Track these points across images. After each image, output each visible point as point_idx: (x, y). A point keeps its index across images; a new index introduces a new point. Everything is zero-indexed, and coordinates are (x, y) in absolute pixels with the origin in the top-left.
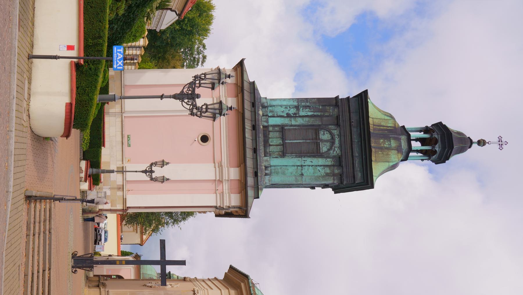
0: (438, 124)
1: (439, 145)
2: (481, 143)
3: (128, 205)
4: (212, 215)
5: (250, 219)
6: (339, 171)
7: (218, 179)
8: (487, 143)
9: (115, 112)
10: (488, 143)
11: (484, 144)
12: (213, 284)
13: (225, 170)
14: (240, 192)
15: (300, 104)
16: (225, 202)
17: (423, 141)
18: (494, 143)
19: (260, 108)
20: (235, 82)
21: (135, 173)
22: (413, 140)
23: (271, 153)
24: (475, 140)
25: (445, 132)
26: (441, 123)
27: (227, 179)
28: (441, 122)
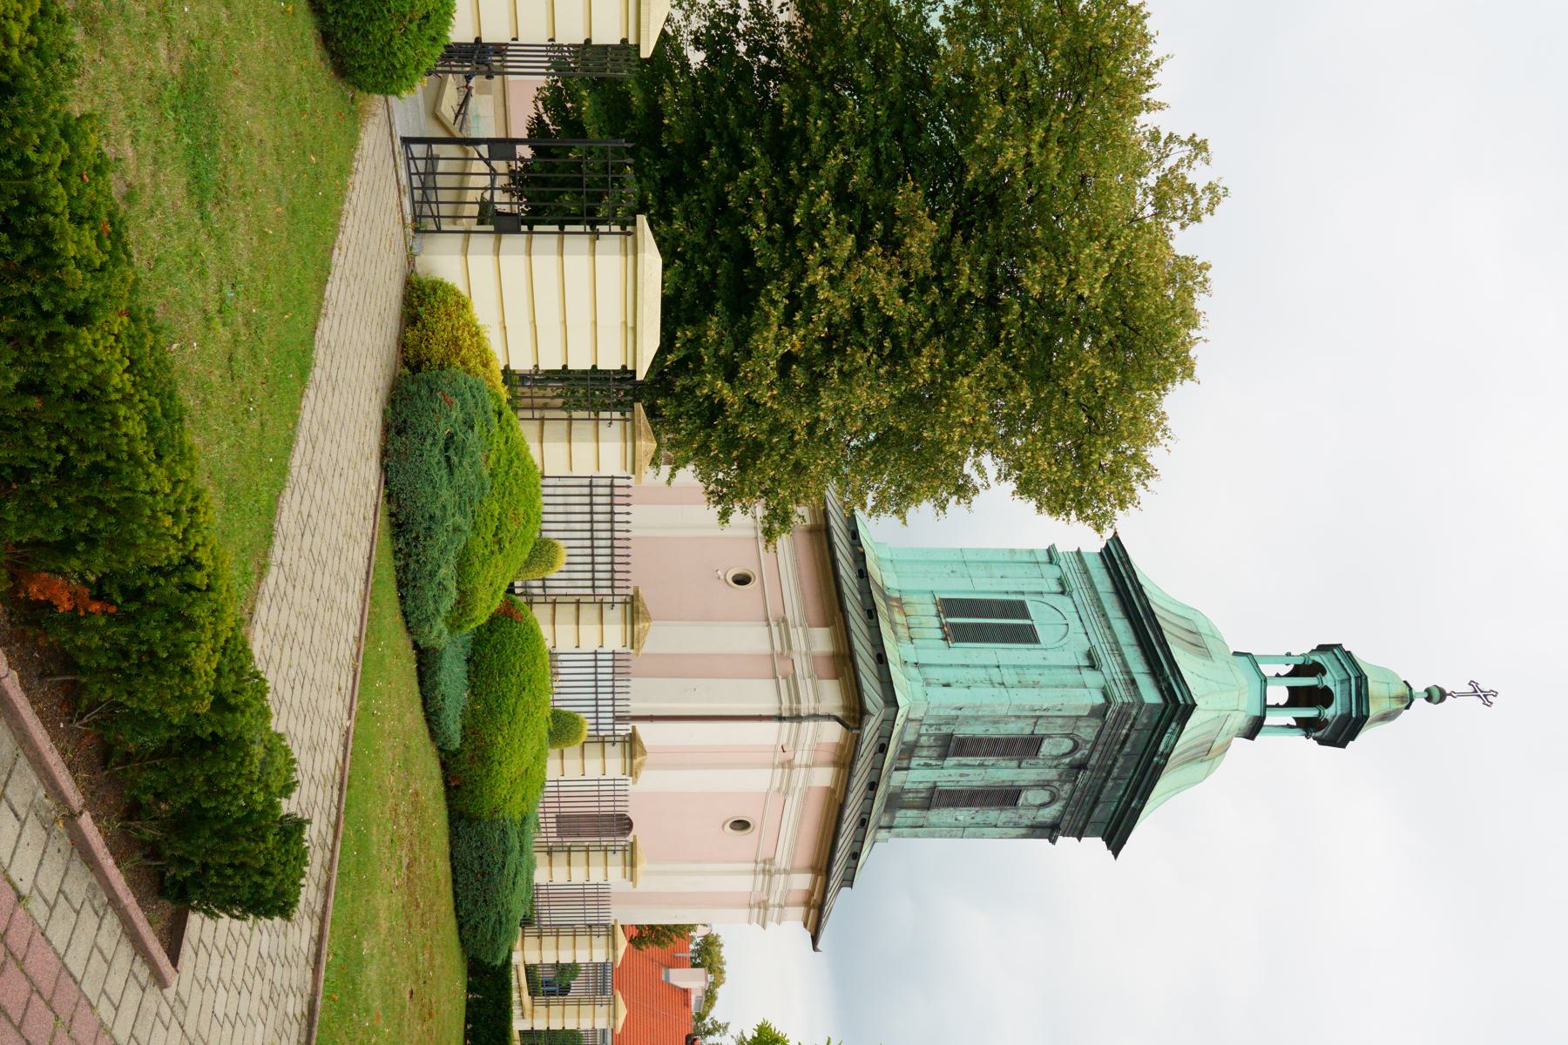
2: (1436, 696)
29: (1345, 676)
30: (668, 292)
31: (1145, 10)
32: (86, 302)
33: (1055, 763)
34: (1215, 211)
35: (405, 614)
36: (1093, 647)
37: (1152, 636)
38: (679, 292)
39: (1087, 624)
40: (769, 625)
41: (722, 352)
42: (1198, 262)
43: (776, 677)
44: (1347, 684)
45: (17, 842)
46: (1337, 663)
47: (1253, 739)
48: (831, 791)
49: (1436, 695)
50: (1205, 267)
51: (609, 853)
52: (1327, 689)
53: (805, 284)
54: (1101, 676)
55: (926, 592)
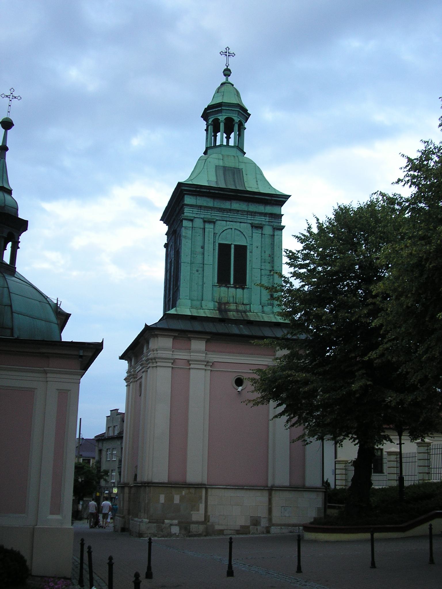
2: (227, 72)
7: (171, 364)
8: (227, 67)
10: (227, 66)
11: (229, 70)
13: (194, 356)
14: (189, 339)
16: (199, 358)
18: (227, 60)
27: (204, 355)
36: (251, 224)
37: (247, 195)
40: (156, 367)
44: (240, 113)
49: (226, 72)
52: (226, 119)
54: (196, 220)
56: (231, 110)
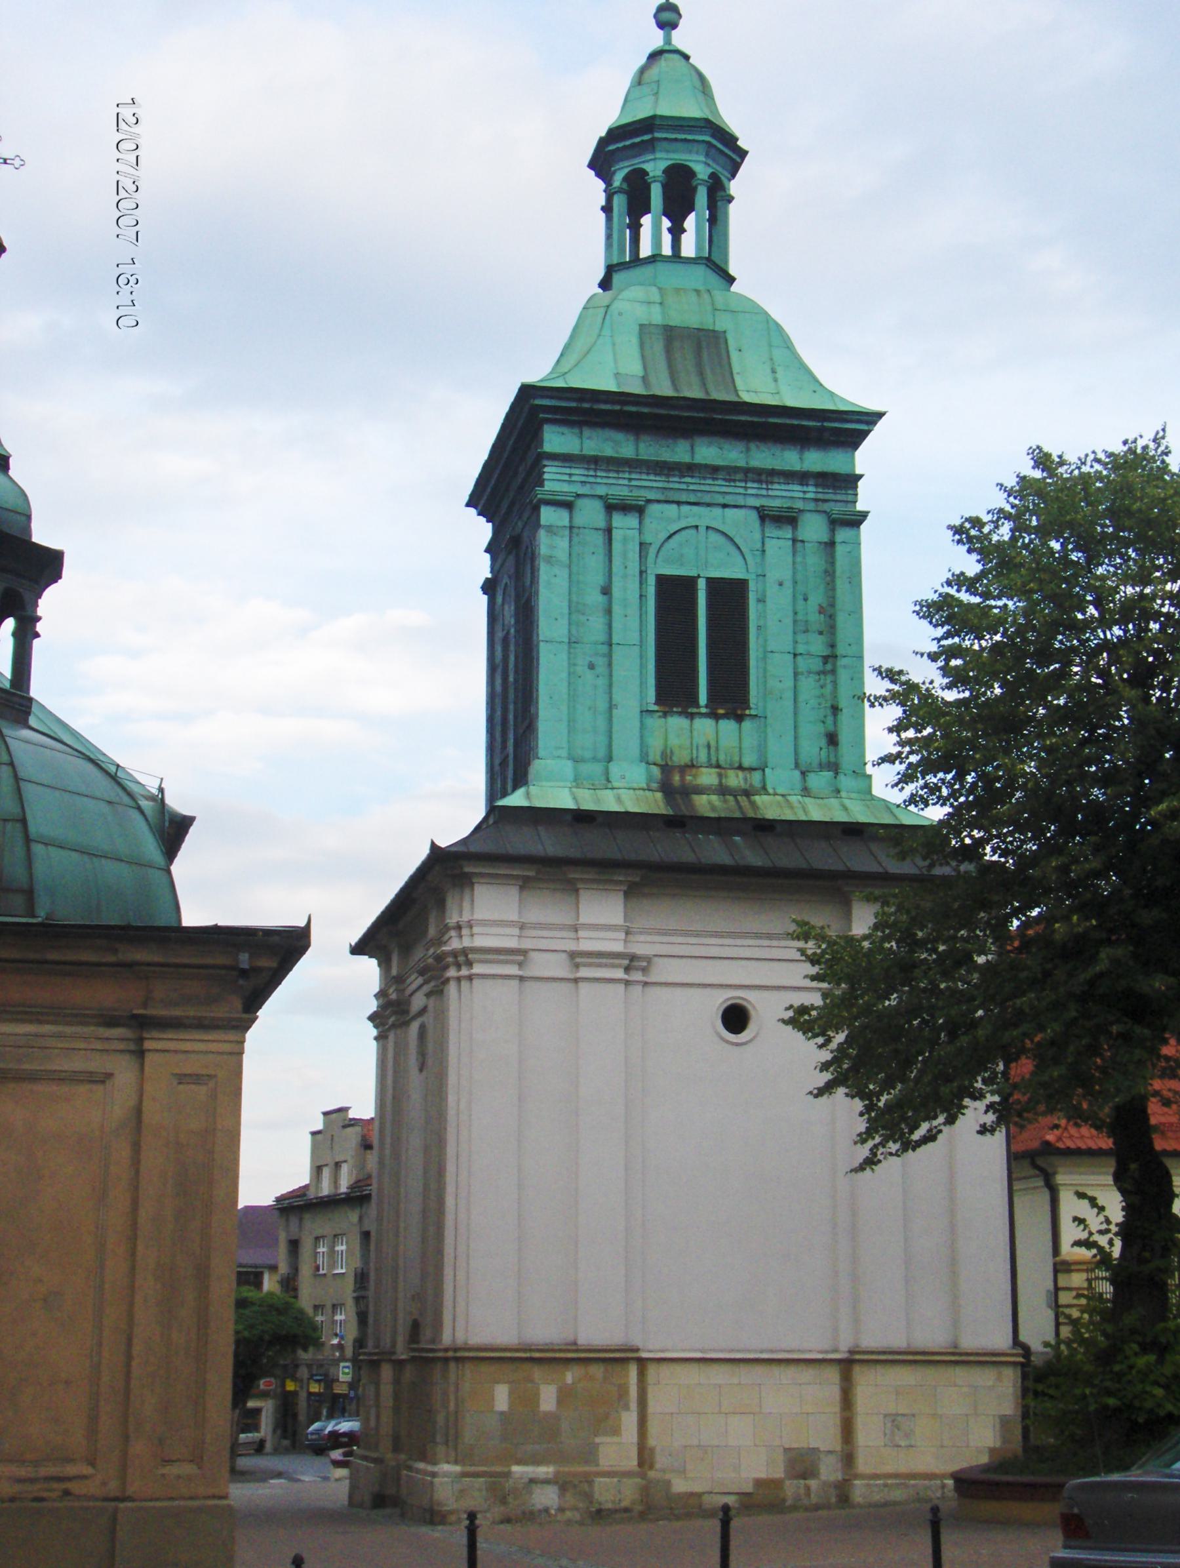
0: (864, 427)
1: (644, 162)
3: (1001, 1340)
4: (691, 61)
5: (879, 431)
6: (1105, 1130)
9: (614, 641)
12: (1019, 1282)
15: (1091, 709)
17: (677, 210)
19: (986, 955)
20: (621, 896)
21: (930, 1145)
22: (693, 457)
23: (813, 528)
24: (656, 38)
25: (707, 138)
26: (488, 550)
27: (622, 935)
28: (591, 165)
29: (702, 147)
30: (721, 193)
31: (964, 1111)
32: (1091, 1311)
33: (706, 296)
34: (809, 1096)
35: (569, 683)
38: (188, 932)
39: (707, 499)
41: (1031, 932)
42: (897, 669)
43: (576, 981)
45: (454, 1327)
46: (679, 145)
47: (743, 154)
48: (632, 892)
50: (725, 332)
51: (463, 983)
52: (668, 171)
53: (998, 638)
55: (642, 725)
56: (686, 140)
